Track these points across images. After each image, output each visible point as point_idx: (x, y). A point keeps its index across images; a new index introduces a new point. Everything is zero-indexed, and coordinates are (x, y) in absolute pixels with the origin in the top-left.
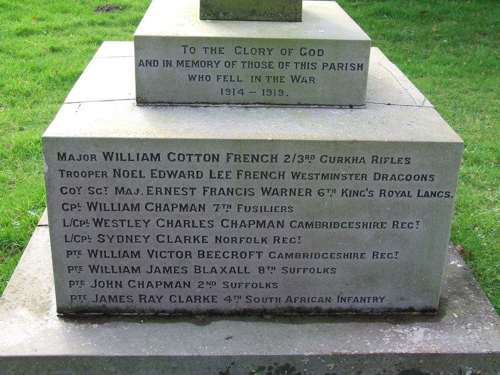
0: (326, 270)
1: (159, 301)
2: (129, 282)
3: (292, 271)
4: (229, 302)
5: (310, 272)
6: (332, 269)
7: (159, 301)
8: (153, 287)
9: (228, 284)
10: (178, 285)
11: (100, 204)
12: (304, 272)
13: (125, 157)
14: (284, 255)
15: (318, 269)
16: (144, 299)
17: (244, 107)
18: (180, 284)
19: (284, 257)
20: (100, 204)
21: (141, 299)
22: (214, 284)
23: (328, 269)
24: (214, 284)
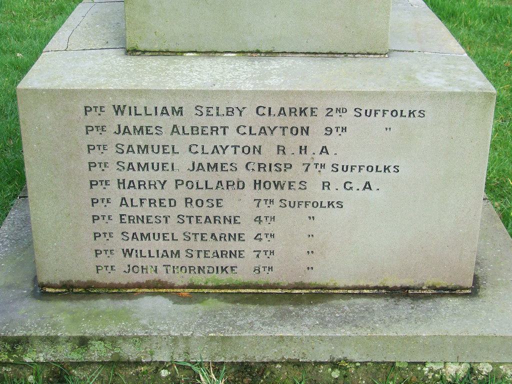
0: (386, 169)
1: (224, 153)
2: (202, 206)
3: (368, 114)
4: (260, 223)
5: (367, 170)
6: (394, 167)
7: (224, 153)
8: (127, 206)
9: (193, 253)
10: (132, 185)
11: (130, 108)
12: (360, 171)
13: (141, 110)
14: (170, 110)
15: (377, 167)
16: (264, 168)
17: (329, 289)
18: (133, 183)
19: (170, 113)
20: (130, 108)
21: (278, 149)
22: (344, 110)
23: (389, 166)
24: (344, 110)
